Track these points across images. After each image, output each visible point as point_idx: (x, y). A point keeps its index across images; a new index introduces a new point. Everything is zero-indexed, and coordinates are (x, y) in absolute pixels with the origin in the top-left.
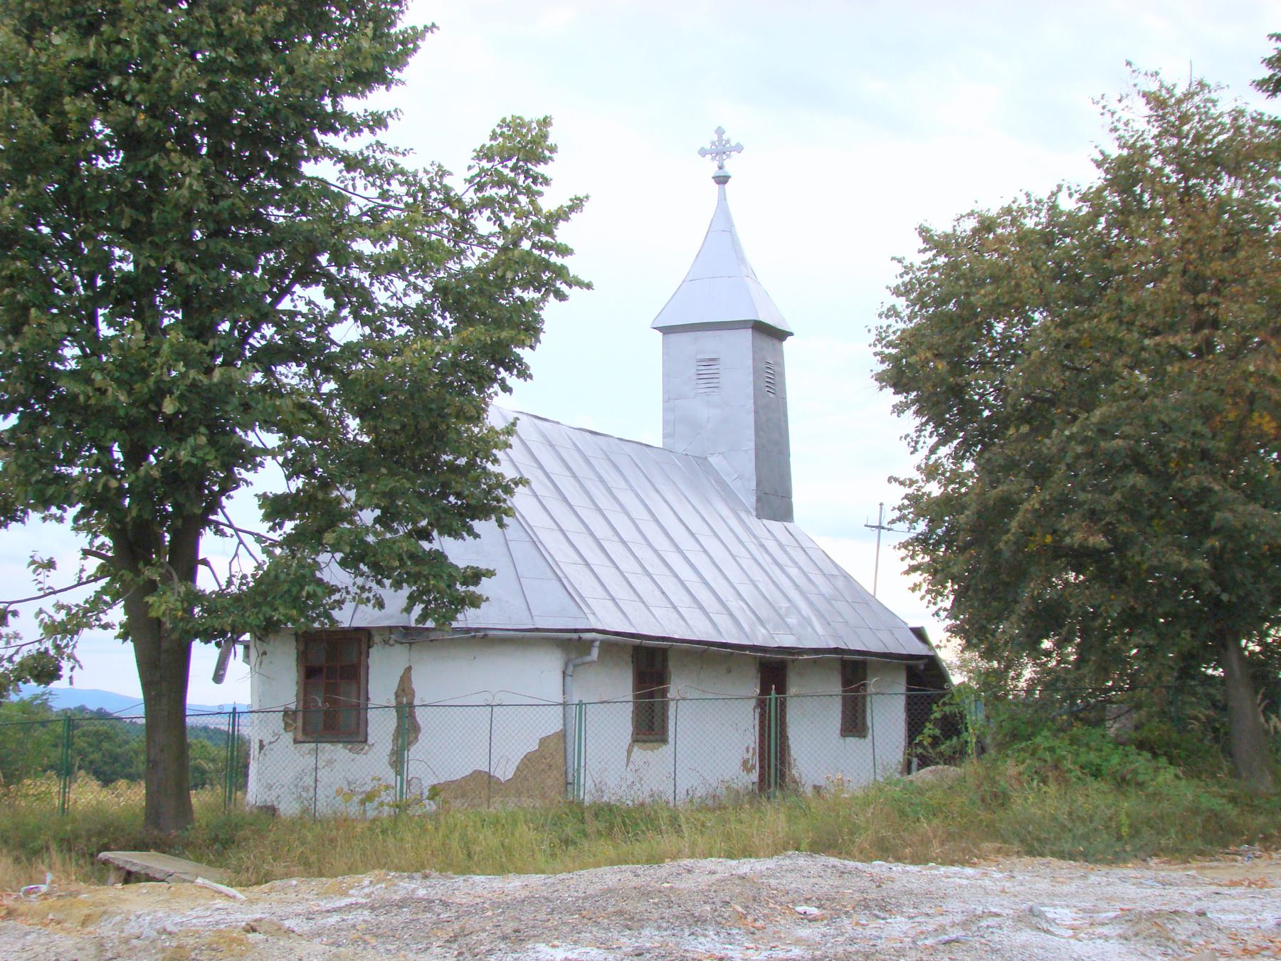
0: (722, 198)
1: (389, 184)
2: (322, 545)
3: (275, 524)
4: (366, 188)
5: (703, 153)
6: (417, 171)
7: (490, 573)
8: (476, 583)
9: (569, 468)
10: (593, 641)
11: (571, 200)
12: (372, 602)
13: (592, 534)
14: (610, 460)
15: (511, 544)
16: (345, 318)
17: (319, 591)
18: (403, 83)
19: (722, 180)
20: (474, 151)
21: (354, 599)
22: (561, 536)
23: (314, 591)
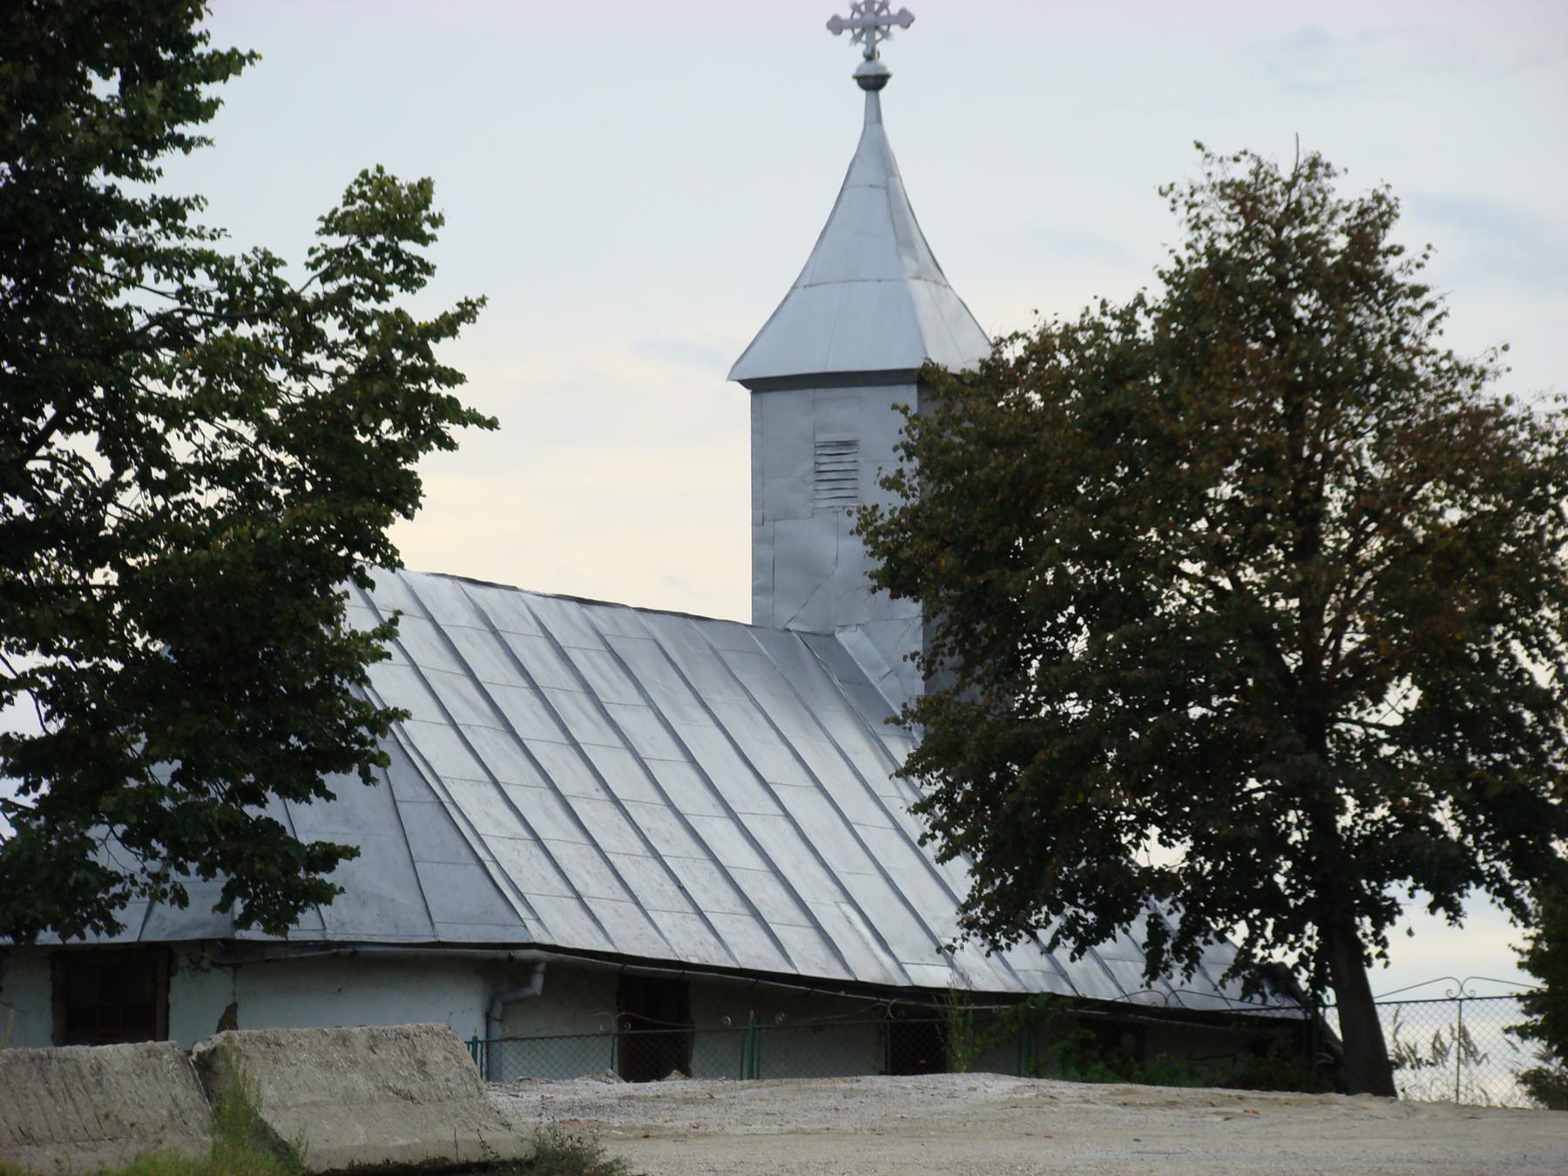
0: (874, 117)
1: (192, 275)
2: (96, 812)
3: (27, 783)
4: (157, 280)
5: (836, 26)
6: (232, 259)
7: (351, 853)
8: (330, 868)
9: (524, 673)
10: (535, 962)
11: (459, 305)
12: (170, 896)
13: (554, 788)
14: (612, 651)
15: (401, 807)
16: (129, 484)
17: (93, 878)
18: (209, 143)
19: (873, 82)
20: (321, 219)
21: (143, 893)
22: (492, 792)
23: (86, 878)
